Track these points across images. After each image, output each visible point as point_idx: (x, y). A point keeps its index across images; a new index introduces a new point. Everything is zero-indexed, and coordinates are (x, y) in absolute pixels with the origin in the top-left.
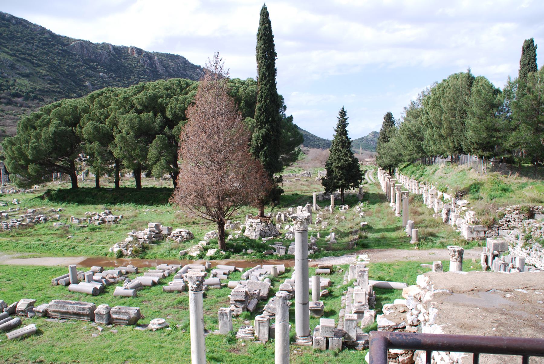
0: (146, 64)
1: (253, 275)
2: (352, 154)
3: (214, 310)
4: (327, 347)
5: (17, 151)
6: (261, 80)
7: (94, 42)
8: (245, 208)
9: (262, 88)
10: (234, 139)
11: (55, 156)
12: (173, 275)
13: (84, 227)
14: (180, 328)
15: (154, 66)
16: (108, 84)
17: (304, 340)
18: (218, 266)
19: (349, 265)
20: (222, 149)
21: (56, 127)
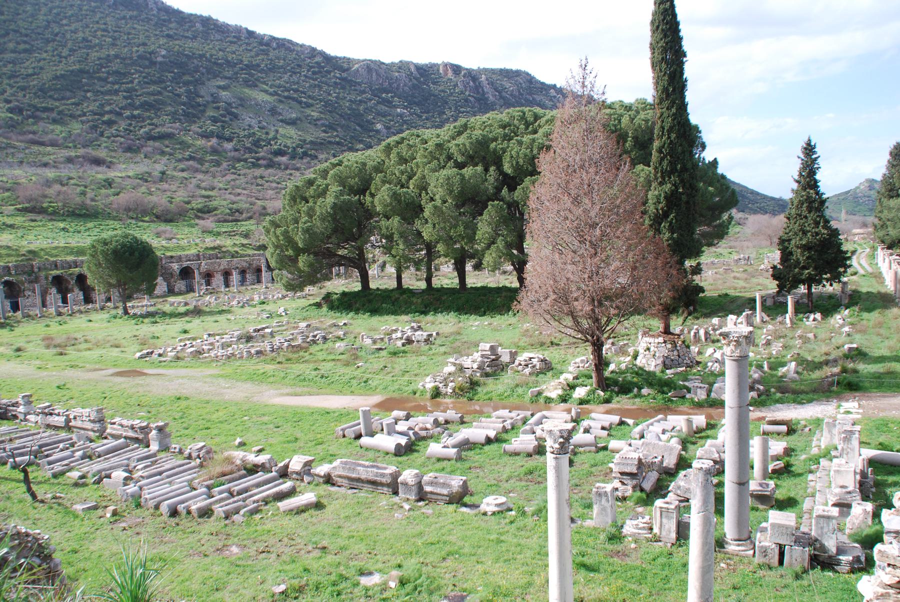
0: (468, 88)
1: (650, 432)
2: (827, 222)
3: (587, 487)
4: (781, 562)
5: (283, 235)
6: (660, 100)
7: (387, 60)
8: (636, 318)
9: (662, 114)
10: (618, 202)
11: (336, 241)
12: (520, 428)
13: (380, 349)
14: (530, 513)
15: (480, 90)
16: (411, 126)
17: (739, 545)
18: (593, 415)
19: (823, 420)
20: (597, 220)
21: (337, 197)
